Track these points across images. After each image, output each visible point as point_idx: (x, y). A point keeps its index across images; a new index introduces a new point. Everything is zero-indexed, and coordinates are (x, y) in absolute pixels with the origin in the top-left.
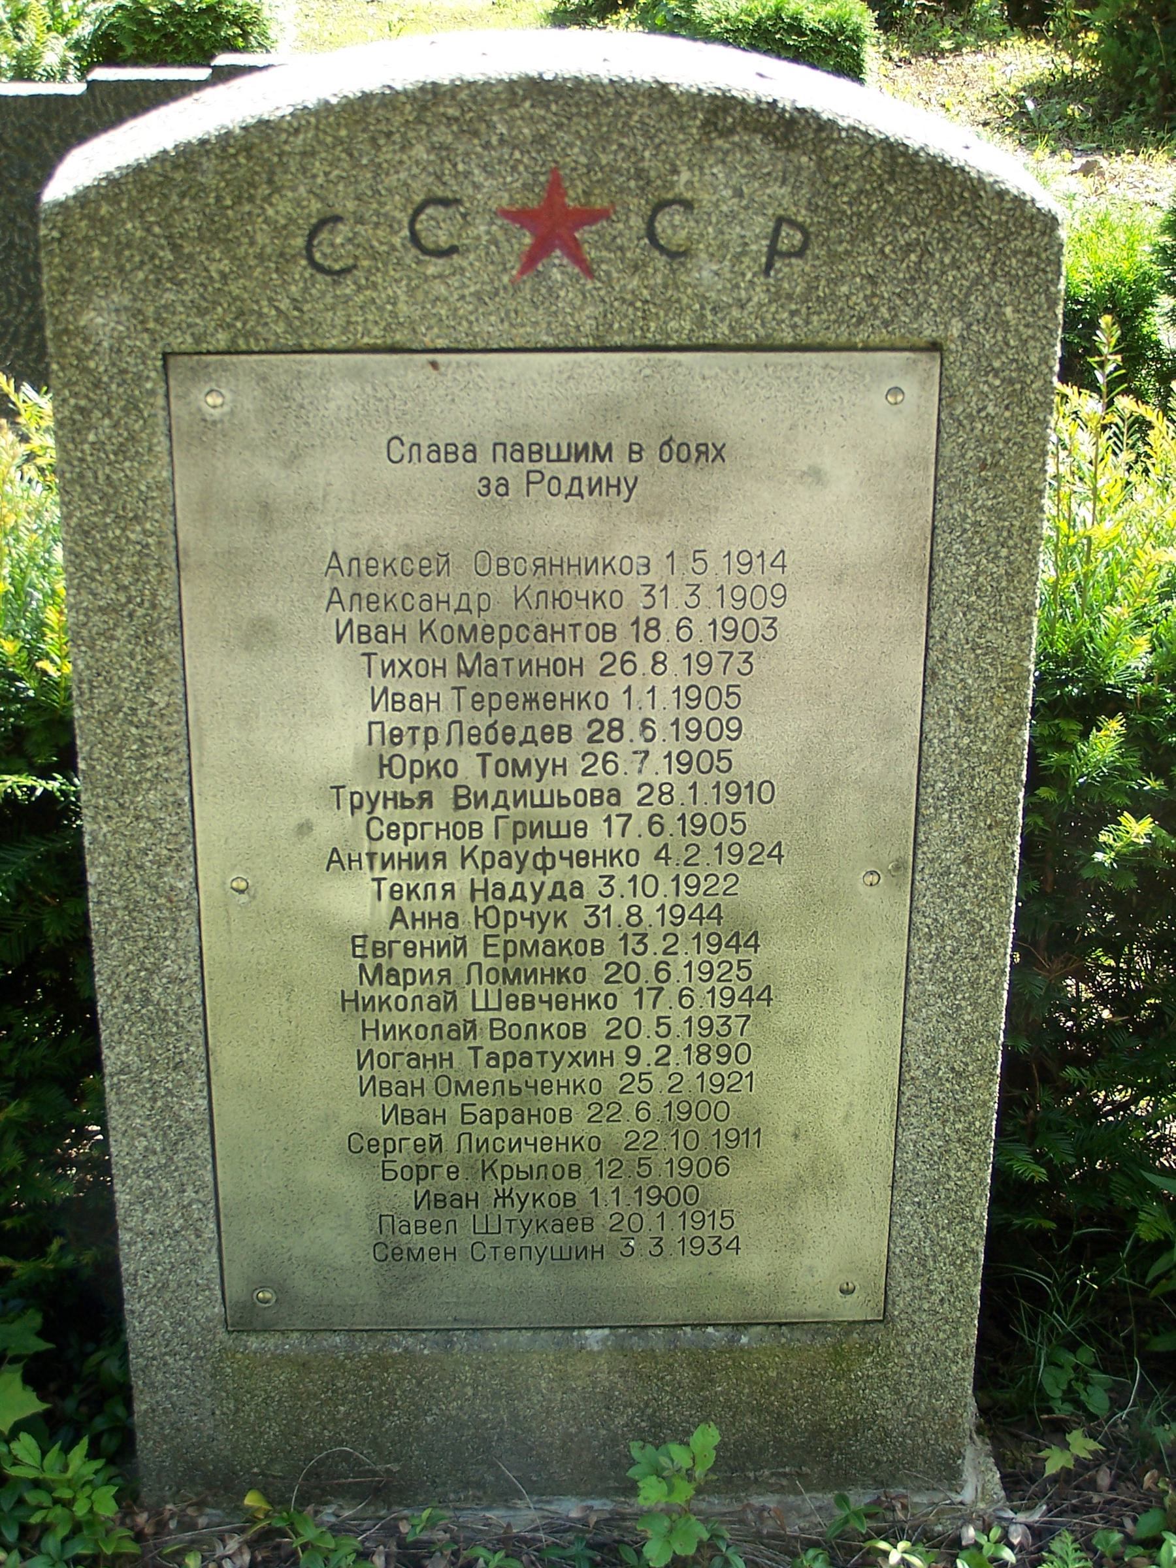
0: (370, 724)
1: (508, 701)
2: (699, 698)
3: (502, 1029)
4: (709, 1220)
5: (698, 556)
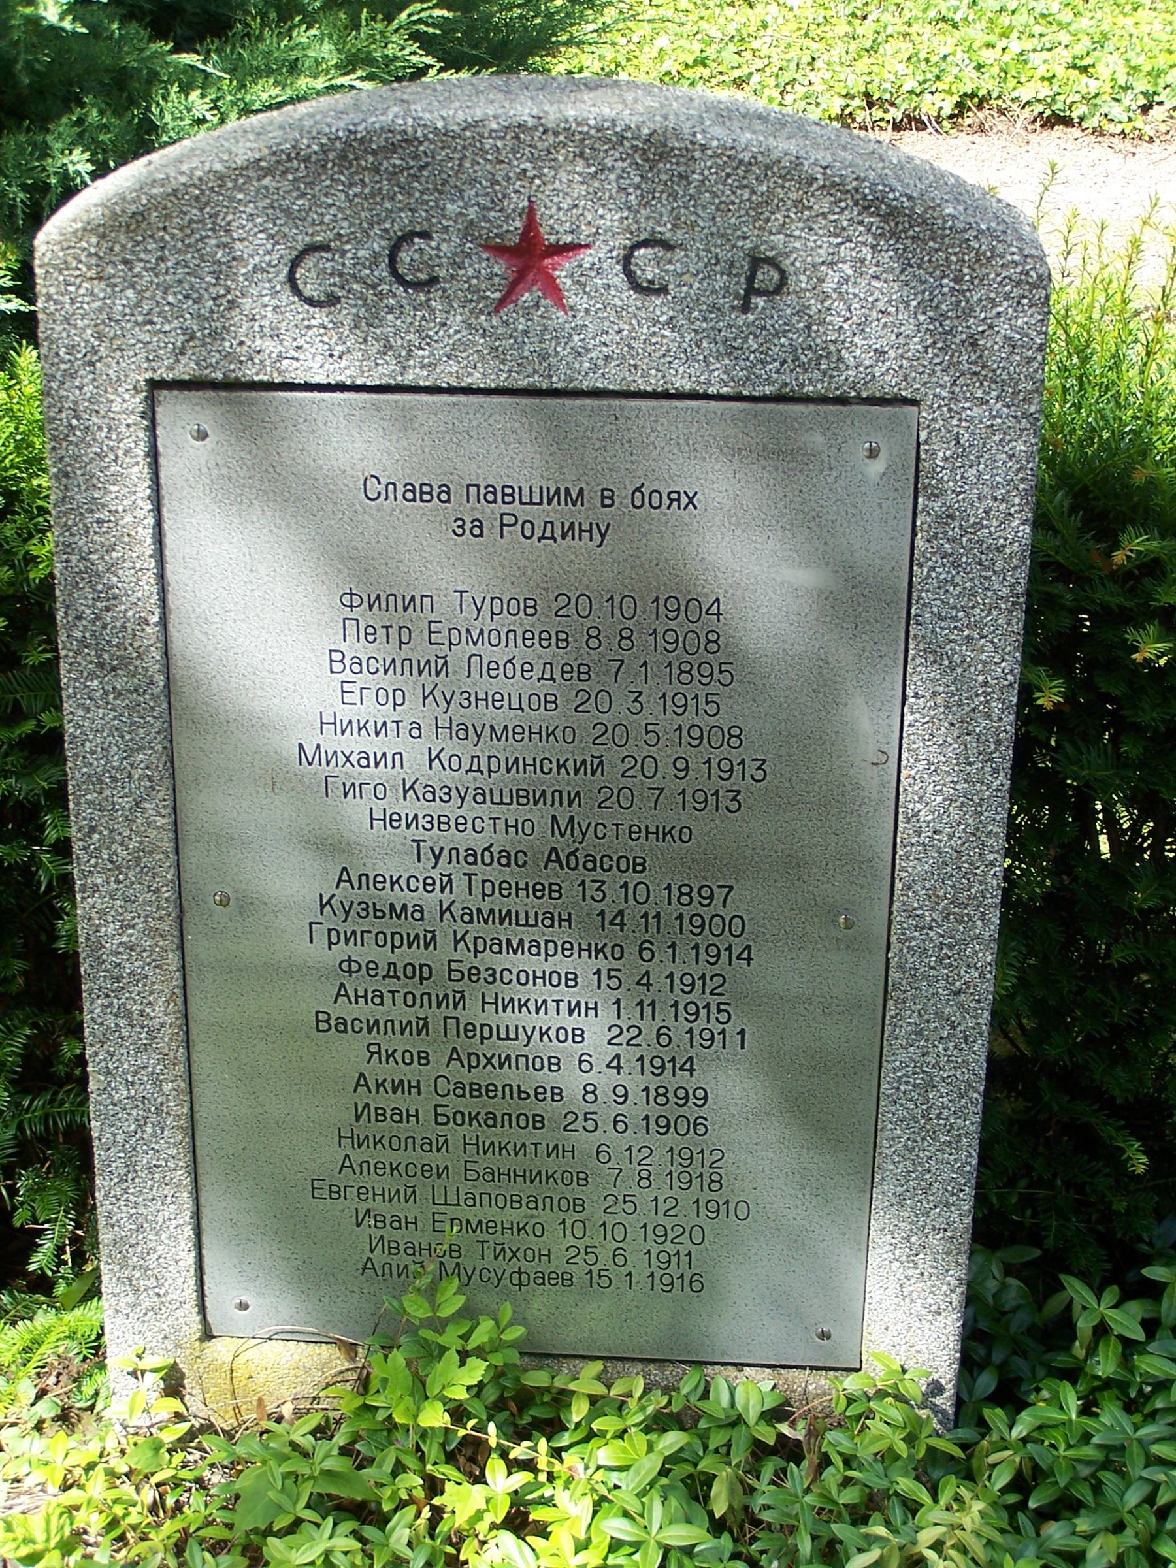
1: (501, 889)
2: (701, 737)
3: (327, 1021)
4: (703, 1012)
5: (724, 668)
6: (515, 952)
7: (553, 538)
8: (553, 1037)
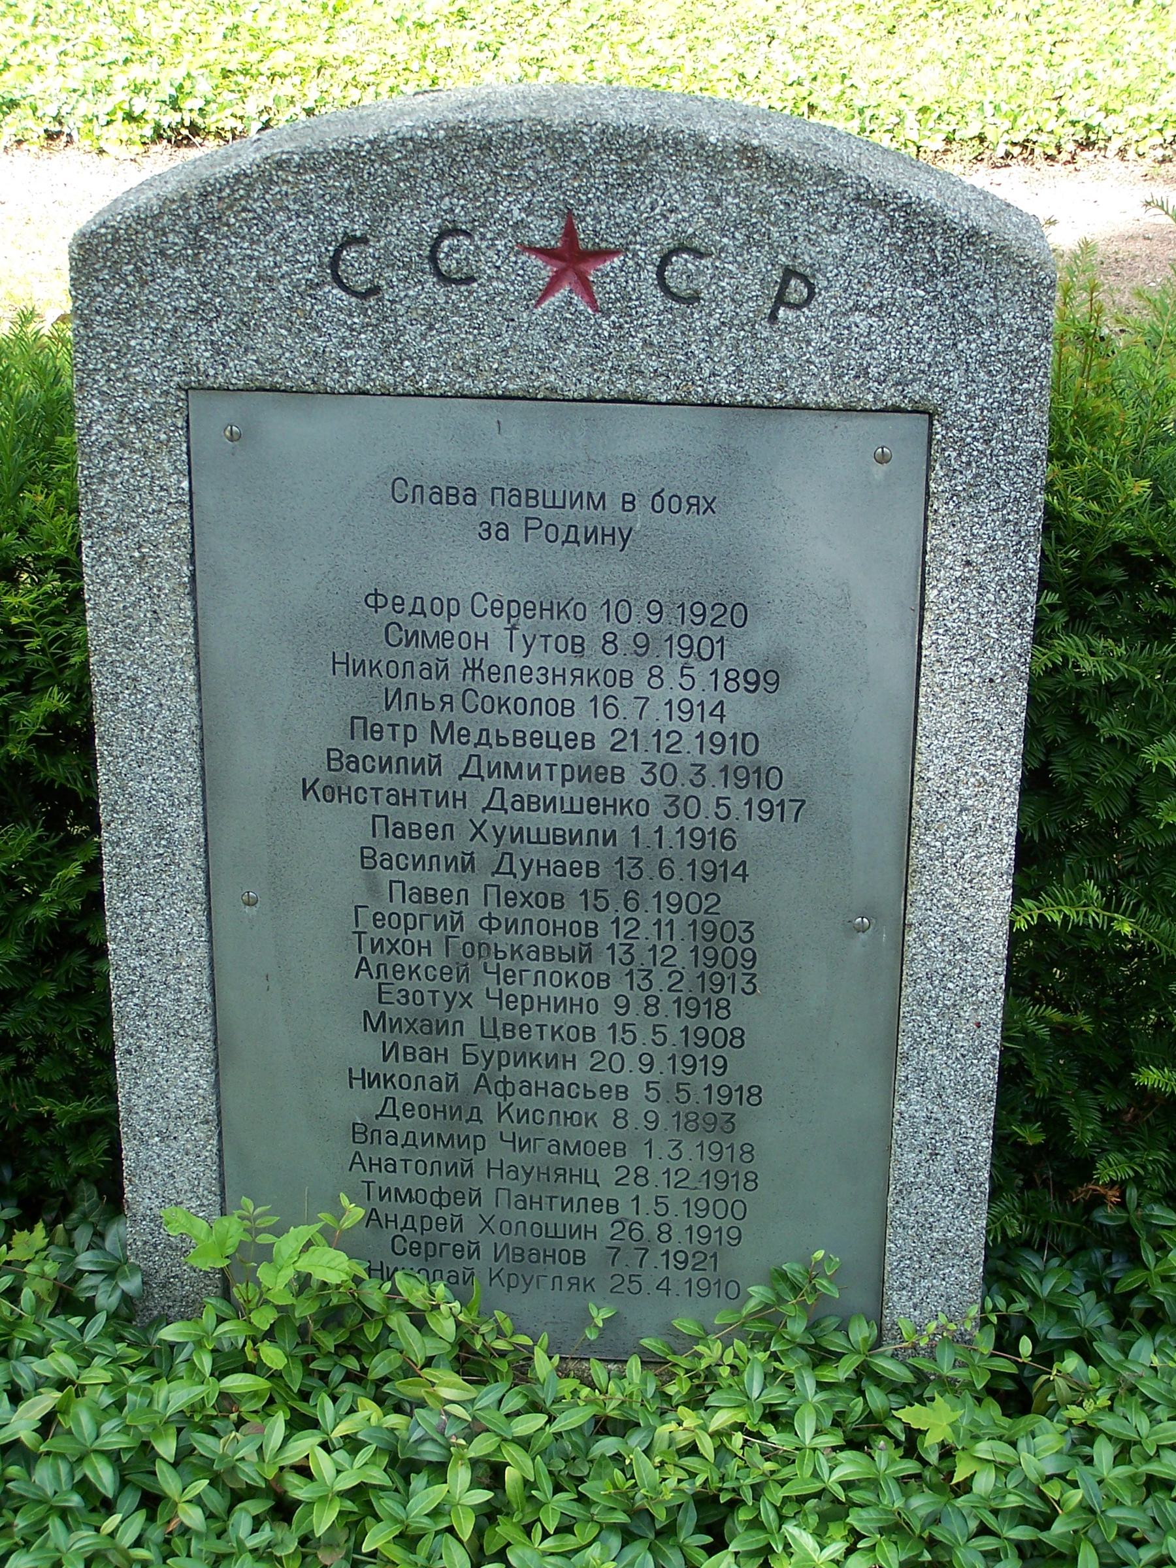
0: (374, 817)
3: (339, 759)
5: (686, 671)
6: (513, 777)
7: (576, 542)
8: (511, 708)
